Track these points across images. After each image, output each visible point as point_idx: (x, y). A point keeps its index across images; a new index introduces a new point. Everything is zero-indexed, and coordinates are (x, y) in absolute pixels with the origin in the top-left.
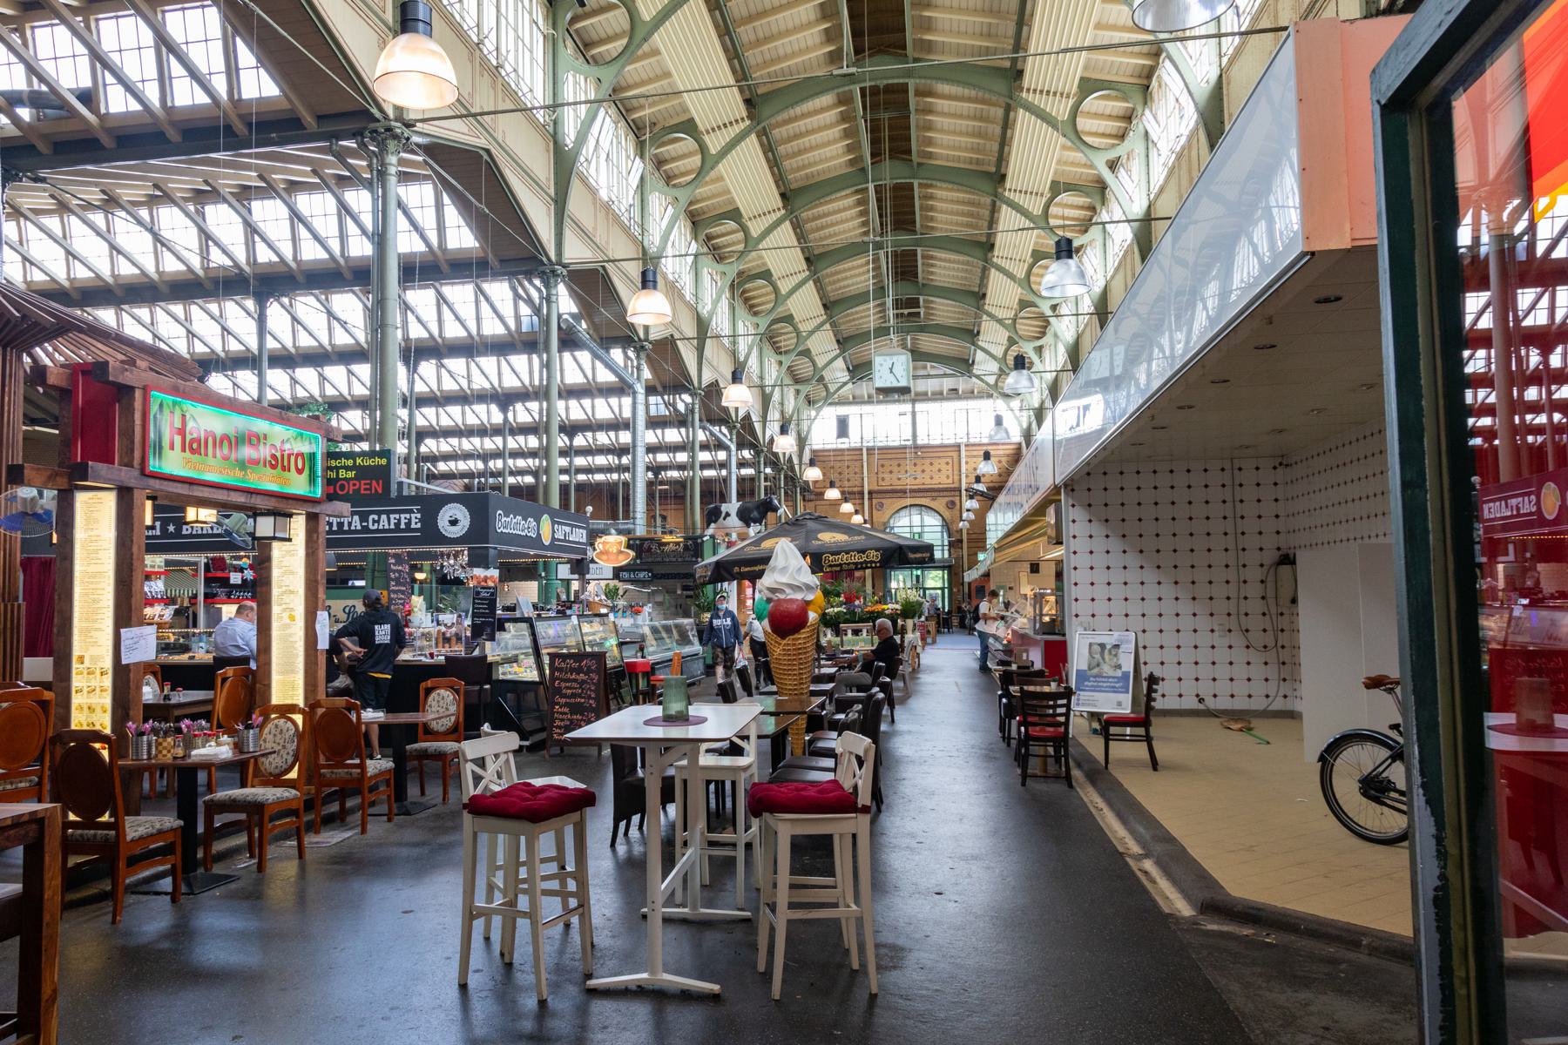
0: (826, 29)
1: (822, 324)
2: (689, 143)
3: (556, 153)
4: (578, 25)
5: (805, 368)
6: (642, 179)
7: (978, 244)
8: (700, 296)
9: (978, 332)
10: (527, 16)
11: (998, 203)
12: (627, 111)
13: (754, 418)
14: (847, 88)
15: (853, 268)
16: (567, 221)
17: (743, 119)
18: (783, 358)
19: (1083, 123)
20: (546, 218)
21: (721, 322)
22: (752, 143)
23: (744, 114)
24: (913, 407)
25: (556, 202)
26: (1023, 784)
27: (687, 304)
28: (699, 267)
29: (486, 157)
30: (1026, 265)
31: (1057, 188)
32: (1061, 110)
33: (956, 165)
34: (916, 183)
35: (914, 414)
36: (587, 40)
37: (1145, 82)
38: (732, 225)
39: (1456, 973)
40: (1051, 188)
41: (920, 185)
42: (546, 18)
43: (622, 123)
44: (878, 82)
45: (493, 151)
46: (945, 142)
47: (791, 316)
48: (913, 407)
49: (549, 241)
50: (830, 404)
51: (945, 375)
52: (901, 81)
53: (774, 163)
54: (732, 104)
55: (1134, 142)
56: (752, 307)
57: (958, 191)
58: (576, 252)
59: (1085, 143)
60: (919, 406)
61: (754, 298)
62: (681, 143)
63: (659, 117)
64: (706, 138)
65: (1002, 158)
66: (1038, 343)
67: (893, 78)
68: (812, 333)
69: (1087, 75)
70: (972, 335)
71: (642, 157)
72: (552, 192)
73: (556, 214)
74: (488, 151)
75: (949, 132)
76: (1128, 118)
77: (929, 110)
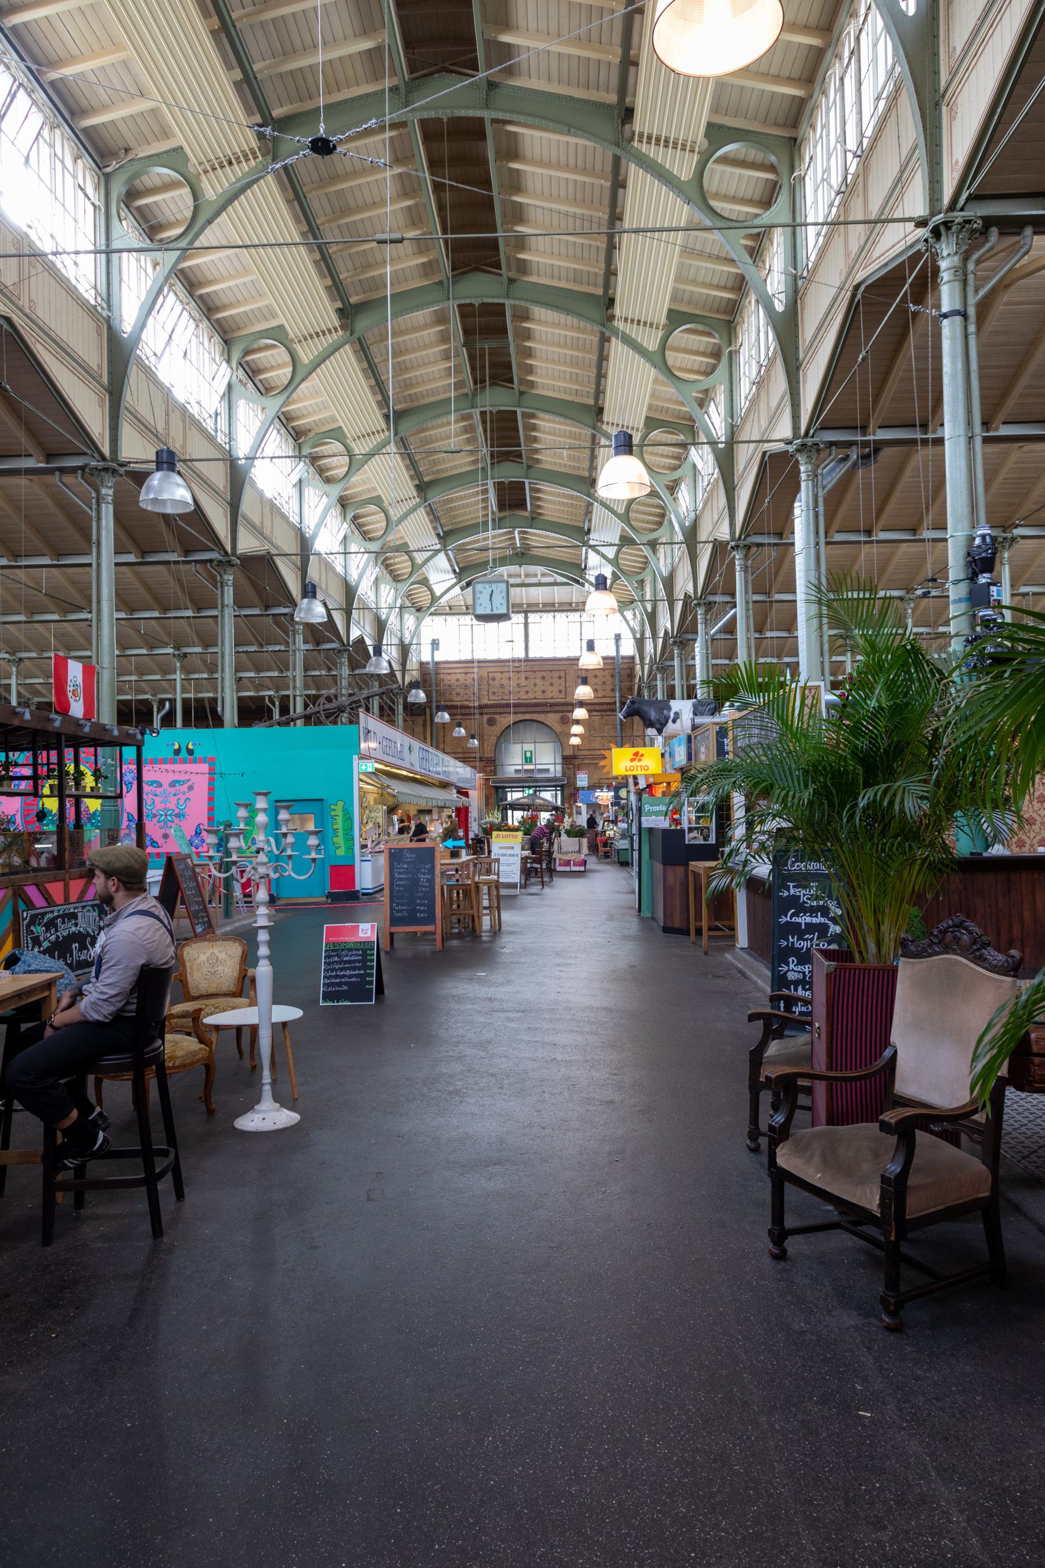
0: (441, 331)
1: (385, 443)
2: (336, 447)
3: (109, 339)
4: (249, 358)
5: (424, 598)
6: (230, 386)
7: (580, 479)
8: (233, 436)
9: (589, 530)
10: (69, 179)
11: (598, 435)
12: (253, 372)
13: (368, 641)
14: (469, 411)
15: (466, 497)
16: (124, 414)
17: (383, 431)
18: (399, 585)
19: (671, 357)
20: (99, 411)
21: (365, 590)
22: (347, 355)
23: (337, 324)
24: (526, 618)
25: (111, 393)
26: (781, 1256)
27: (337, 575)
28: (234, 397)
29: (6, 326)
30: (660, 333)
31: (676, 318)
32: (651, 341)
33: (555, 283)
34: (527, 481)
35: (526, 624)
36: (268, 386)
37: (728, 318)
38: (373, 508)
39: (111, 492)
40: (668, 318)
41: (524, 414)
42: (97, 187)
43: (283, 430)
44: (473, 301)
45: (15, 319)
46: (547, 429)
47: (406, 544)
48: (526, 618)
49: (226, 537)
50: (431, 614)
51: (555, 584)
52: (496, 301)
53: (412, 465)
54: (325, 313)
55: (685, 470)
56: (365, 532)
57: (560, 423)
58: (247, 544)
59: (679, 378)
60: (532, 617)
61: (395, 564)
62: (274, 351)
63: (314, 426)
64: (298, 347)
65: (599, 392)
66: (640, 577)
67: (488, 297)
68: (370, 455)
69: (675, 307)
70: (581, 533)
71: (228, 361)
72: (105, 380)
73: (231, 515)
74: (8, 320)
75: (549, 434)
76: (716, 354)
77: (535, 439)
